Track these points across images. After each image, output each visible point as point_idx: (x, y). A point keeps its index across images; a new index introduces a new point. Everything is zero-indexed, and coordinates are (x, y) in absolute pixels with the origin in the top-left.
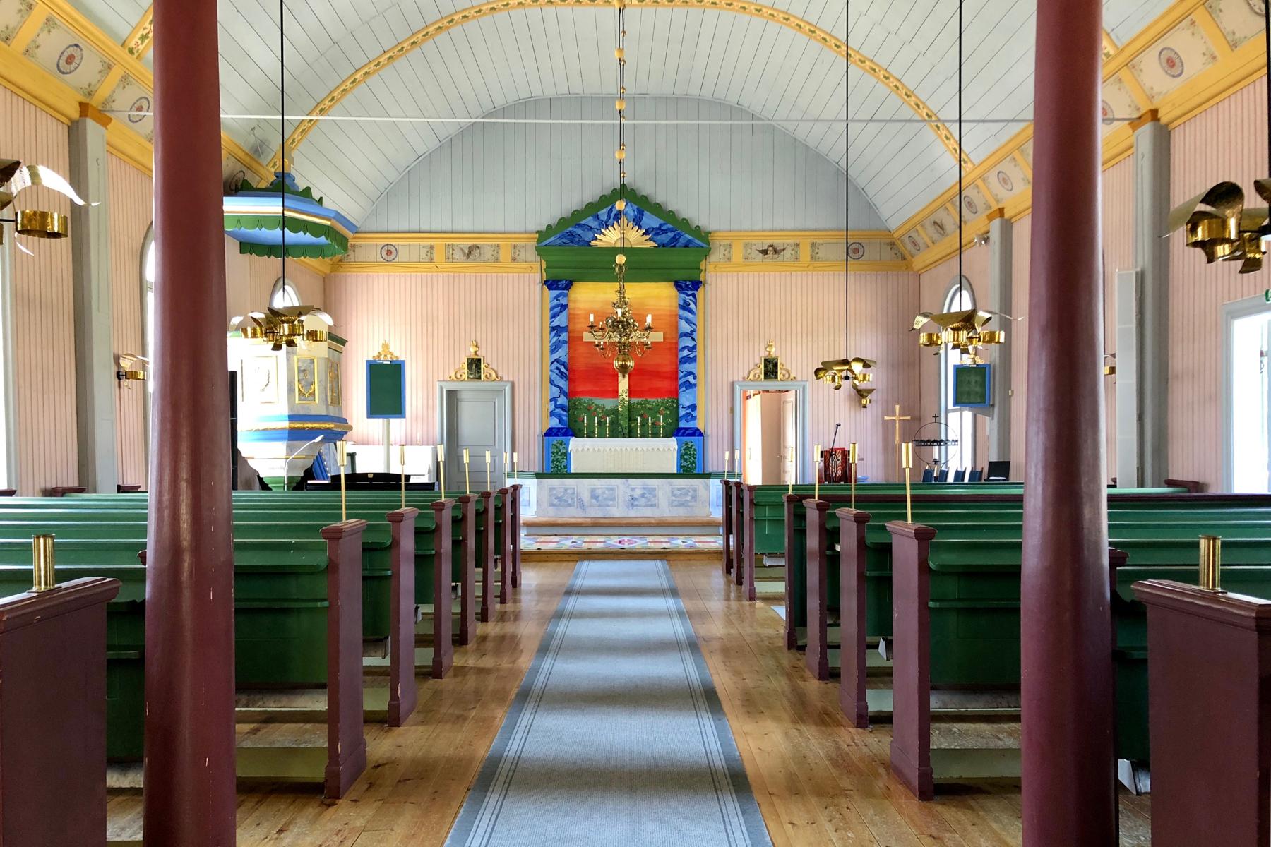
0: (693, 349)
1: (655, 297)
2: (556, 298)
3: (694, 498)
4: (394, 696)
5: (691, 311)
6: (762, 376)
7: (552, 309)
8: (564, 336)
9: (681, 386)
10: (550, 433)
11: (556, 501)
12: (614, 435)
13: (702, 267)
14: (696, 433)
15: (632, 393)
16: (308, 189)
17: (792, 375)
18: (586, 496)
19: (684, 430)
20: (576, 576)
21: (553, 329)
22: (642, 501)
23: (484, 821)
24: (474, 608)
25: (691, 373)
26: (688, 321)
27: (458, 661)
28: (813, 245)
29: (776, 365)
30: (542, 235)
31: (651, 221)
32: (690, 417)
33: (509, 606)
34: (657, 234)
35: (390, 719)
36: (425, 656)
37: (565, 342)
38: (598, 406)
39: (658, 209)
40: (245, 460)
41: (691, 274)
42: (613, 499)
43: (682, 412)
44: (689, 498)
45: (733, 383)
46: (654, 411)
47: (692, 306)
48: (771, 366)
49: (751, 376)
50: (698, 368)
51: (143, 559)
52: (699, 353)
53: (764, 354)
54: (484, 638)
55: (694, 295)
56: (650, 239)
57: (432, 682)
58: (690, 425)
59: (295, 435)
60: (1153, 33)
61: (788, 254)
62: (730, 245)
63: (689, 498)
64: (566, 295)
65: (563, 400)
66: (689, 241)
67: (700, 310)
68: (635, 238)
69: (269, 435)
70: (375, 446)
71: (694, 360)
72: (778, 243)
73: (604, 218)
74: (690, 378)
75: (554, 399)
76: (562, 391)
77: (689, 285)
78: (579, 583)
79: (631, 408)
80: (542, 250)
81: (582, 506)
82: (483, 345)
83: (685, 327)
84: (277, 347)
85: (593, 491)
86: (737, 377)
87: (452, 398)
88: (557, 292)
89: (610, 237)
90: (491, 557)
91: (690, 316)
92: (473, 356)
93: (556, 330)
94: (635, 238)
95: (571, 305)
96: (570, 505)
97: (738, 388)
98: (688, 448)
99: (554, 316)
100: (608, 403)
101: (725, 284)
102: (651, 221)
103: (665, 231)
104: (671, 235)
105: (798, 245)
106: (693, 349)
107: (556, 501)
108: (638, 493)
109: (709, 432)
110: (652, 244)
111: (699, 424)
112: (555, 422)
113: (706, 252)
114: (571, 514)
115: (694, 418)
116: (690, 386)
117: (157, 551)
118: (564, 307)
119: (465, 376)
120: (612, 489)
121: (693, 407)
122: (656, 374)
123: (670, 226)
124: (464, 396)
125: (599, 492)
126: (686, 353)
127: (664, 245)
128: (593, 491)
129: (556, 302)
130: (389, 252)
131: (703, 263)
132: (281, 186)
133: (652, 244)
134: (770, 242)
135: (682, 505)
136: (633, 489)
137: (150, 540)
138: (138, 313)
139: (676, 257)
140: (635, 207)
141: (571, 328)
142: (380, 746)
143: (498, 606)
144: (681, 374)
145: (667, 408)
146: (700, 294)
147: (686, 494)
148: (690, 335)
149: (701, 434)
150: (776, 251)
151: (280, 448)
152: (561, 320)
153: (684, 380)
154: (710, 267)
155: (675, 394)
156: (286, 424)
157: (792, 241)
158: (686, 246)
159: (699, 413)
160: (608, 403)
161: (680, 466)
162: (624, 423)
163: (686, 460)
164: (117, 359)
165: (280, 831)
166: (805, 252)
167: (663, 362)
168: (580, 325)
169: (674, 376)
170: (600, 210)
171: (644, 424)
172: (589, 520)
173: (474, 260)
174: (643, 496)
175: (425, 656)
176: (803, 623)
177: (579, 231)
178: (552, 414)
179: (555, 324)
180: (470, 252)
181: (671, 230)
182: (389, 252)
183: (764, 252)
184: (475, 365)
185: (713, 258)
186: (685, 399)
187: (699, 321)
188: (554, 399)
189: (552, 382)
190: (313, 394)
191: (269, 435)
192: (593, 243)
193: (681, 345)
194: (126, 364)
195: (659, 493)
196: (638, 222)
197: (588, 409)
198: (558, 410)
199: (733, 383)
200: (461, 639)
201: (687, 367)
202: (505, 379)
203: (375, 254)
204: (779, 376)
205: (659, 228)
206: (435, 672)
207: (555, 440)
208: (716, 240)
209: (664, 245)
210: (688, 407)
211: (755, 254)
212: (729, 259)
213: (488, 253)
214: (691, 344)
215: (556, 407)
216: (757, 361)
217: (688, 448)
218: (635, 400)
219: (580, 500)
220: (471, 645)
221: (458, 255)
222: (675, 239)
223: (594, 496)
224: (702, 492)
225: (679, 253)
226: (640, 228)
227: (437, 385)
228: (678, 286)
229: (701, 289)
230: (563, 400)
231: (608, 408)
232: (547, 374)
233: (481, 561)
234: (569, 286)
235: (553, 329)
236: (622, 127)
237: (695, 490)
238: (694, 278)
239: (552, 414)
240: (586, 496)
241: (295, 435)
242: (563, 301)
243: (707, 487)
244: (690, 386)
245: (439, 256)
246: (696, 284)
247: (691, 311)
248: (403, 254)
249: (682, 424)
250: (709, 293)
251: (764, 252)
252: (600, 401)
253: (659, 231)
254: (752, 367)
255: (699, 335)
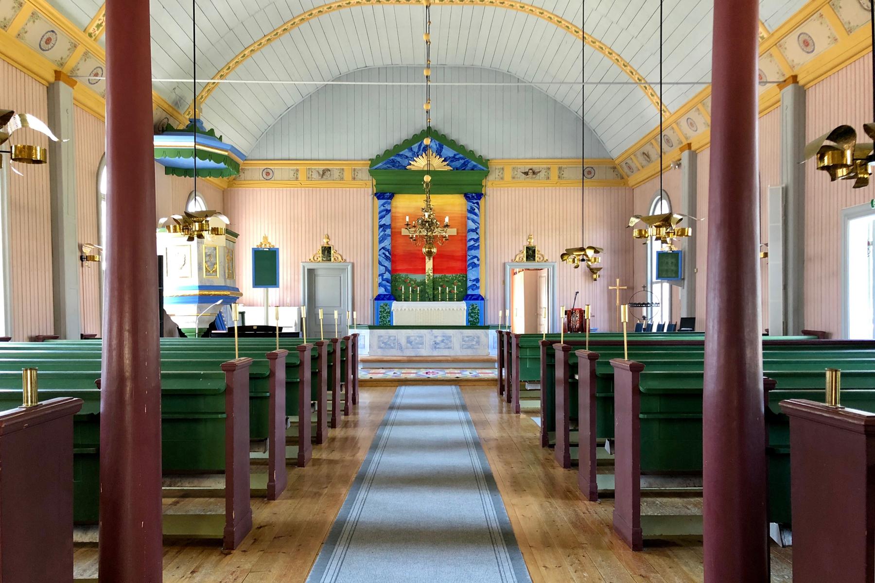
0: (477, 240)
1: (451, 204)
2: (383, 205)
3: (478, 343)
4: (271, 479)
5: (476, 214)
6: (525, 259)
7: (380, 213)
8: (388, 231)
9: (469, 266)
10: (379, 298)
11: (382, 345)
12: (422, 299)
13: (484, 184)
14: (479, 298)
15: (435, 270)
16: (212, 130)
17: (546, 258)
18: (403, 342)
19: (471, 296)
20: (397, 396)
21: (381, 226)
22: (442, 345)
23: (333, 565)
24: (326, 419)
25: (475, 257)
26: (474, 221)
27: (315, 455)
28: (560, 168)
29: (534, 251)
30: (373, 162)
31: (448, 152)
32: (475, 287)
33: (350, 417)
34: (452, 161)
35: (268, 495)
36: (292, 452)
37: (389, 235)
38: (411, 280)
39: (453, 144)
40: (168, 317)
41: (476, 189)
42: (422, 344)
43: (469, 284)
44: (474, 343)
45: (504, 264)
46: (450, 283)
47: (476, 210)
48: (531, 252)
49: (517, 259)
50: (480, 253)
51: (98, 385)
52: (482, 243)
53: (526, 244)
54: (333, 439)
55: (478, 203)
56: (448, 165)
57: (297, 470)
58: (475, 292)
59: (203, 300)
60: (793, 22)
61: (542, 175)
62: (503, 169)
63: (474, 343)
64: (390, 203)
65: (387, 276)
66: (475, 166)
67: (482, 213)
68: (437, 164)
69: (186, 299)
70: (258, 307)
71: (478, 248)
72: (536, 167)
73: (416, 150)
74: (475, 261)
75: (381, 275)
76: (387, 269)
77: (475, 196)
78: (399, 401)
79: (434, 281)
80: (373, 172)
81: (401, 348)
82: (332, 237)
83: (471, 225)
84: (191, 239)
85: (408, 338)
86: (508, 259)
87: (311, 274)
88: (384, 201)
89: (420, 163)
90: (338, 383)
91: (475, 217)
92: (326, 245)
93: (383, 227)
94: (437, 164)
95: (393, 210)
96: (392, 348)
97: (508, 267)
98: (473, 309)
99: (381, 218)
100: (418, 277)
101: (499, 196)
102: (448, 152)
103: (458, 159)
104: (462, 161)
105: (549, 169)
106: (477, 240)
107: (382, 345)
108: (439, 339)
109: (488, 297)
110: (449, 168)
111: (481, 292)
112: (382, 291)
113: (486, 174)
114: (393, 354)
115: (478, 288)
116: (475, 265)
117: (108, 379)
118: (388, 211)
119: (320, 259)
120: (422, 337)
121: (477, 280)
122: (452, 257)
123: (461, 156)
124: (319, 272)
125: (412, 338)
126: (472, 243)
127: (457, 169)
128: (408, 338)
129: (382, 208)
130: (268, 174)
131: (484, 181)
132: (193, 128)
133: (449, 168)
134: (530, 167)
135: (469, 347)
136: (436, 337)
137: (104, 372)
138: (95, 215)
139: (466, 177)
140: (437, 142)
141: (393, 226)
142: (262, 513)
143: (343, 417)
144: (469, 258)
145: (459, 281)
146: (482, 202)
147: (473, 340)
148: (475, 231)
149: (483, 299)
150: (534, 173)
151: (193, 308)
152: (386, 221)
153: (471, 261)
154: (489, 184)
155: (465, 271)
156: (197, 292)
157: (545, 166)
158: (473, 169)
159: (481, 284)
160: (418, 277)
161: (468, 321)
162: (430, 291)
163: (472, 317)
164: (80, 247)
165: (193, 572)
166: (554, 174)
167: (456, 249)
168: (399, 224)
169: (464, 259)
170: (413, 145)
171: (443, 292)
172: (405, 358)
173: (327, 179)
174: (442, 341)
175: (292, 452)
176: (553, 429)
177: (399, 159)
178: (380, 285)
179: (382, 223)
180: (324, 174)
181: (462, 158)
182: (268, 174)
183: (526, 173)
184: (327, 251)
185: (491, 177)
186: (471, 275)
187: (481, 221)
188: (381, 275)
189: (380, 263)
190: (215, 271)
191: (186, 299)
192: (408, 167)
193: (469, 238)
194: (87, 251)
195: (454, 340)
196: (439, 153)
197: (405, 282)
198: (384, 282)
199: (504, 264)
200: (317, 440)
201: (473, 253)
202: (348, 261)
203: (258, 175)
204: (537, 259)
205: (454, 157)
206: (299, 462)
207: (382, 303)
208: (493, 166)
209: (457, 169)
210: (474, 280)
211: (520, 175)
212: (502, 179)
213: (336, 174)
214: (476, 237)
215: (383, 280)
216: (521, 248)
217: (473, 309)
218: (437, 275)
219: (400, 344)
220: (324, 444)
221: (315, 175)
222: (465, 165)
223: (409, 341)
224: (483, 339)
225: (467, 174)
226: (441, 157)
227: (301, 265)
228: (467, 197)
229: (483, 199)
230: (387, 276)
231: (419, 281)
232: (377, 257)
233: (331, 386)
234: (391, 197)
235: (381, 226)
236: (428, 87)
237: (478, 337)
238: (478, 191)
239: (380, 285)
240: (403, 342)
241: (203, 300)
242: (388, 207)
243: (487, 335)
244: (475, 265)
245: (302, 176)
246: (479, 196)
247: (476, 214)
248: (277, 175)
249: (470, 292)
250: (488, 202)
251: (526, 173)
252: (413, 276)
253: (454, 159)
254: (518, 252)
255: (481, 231)
